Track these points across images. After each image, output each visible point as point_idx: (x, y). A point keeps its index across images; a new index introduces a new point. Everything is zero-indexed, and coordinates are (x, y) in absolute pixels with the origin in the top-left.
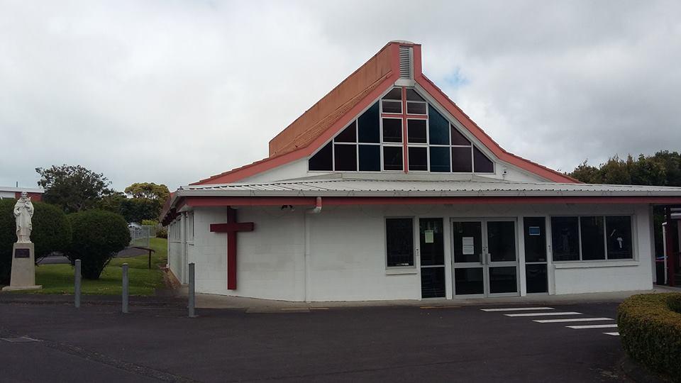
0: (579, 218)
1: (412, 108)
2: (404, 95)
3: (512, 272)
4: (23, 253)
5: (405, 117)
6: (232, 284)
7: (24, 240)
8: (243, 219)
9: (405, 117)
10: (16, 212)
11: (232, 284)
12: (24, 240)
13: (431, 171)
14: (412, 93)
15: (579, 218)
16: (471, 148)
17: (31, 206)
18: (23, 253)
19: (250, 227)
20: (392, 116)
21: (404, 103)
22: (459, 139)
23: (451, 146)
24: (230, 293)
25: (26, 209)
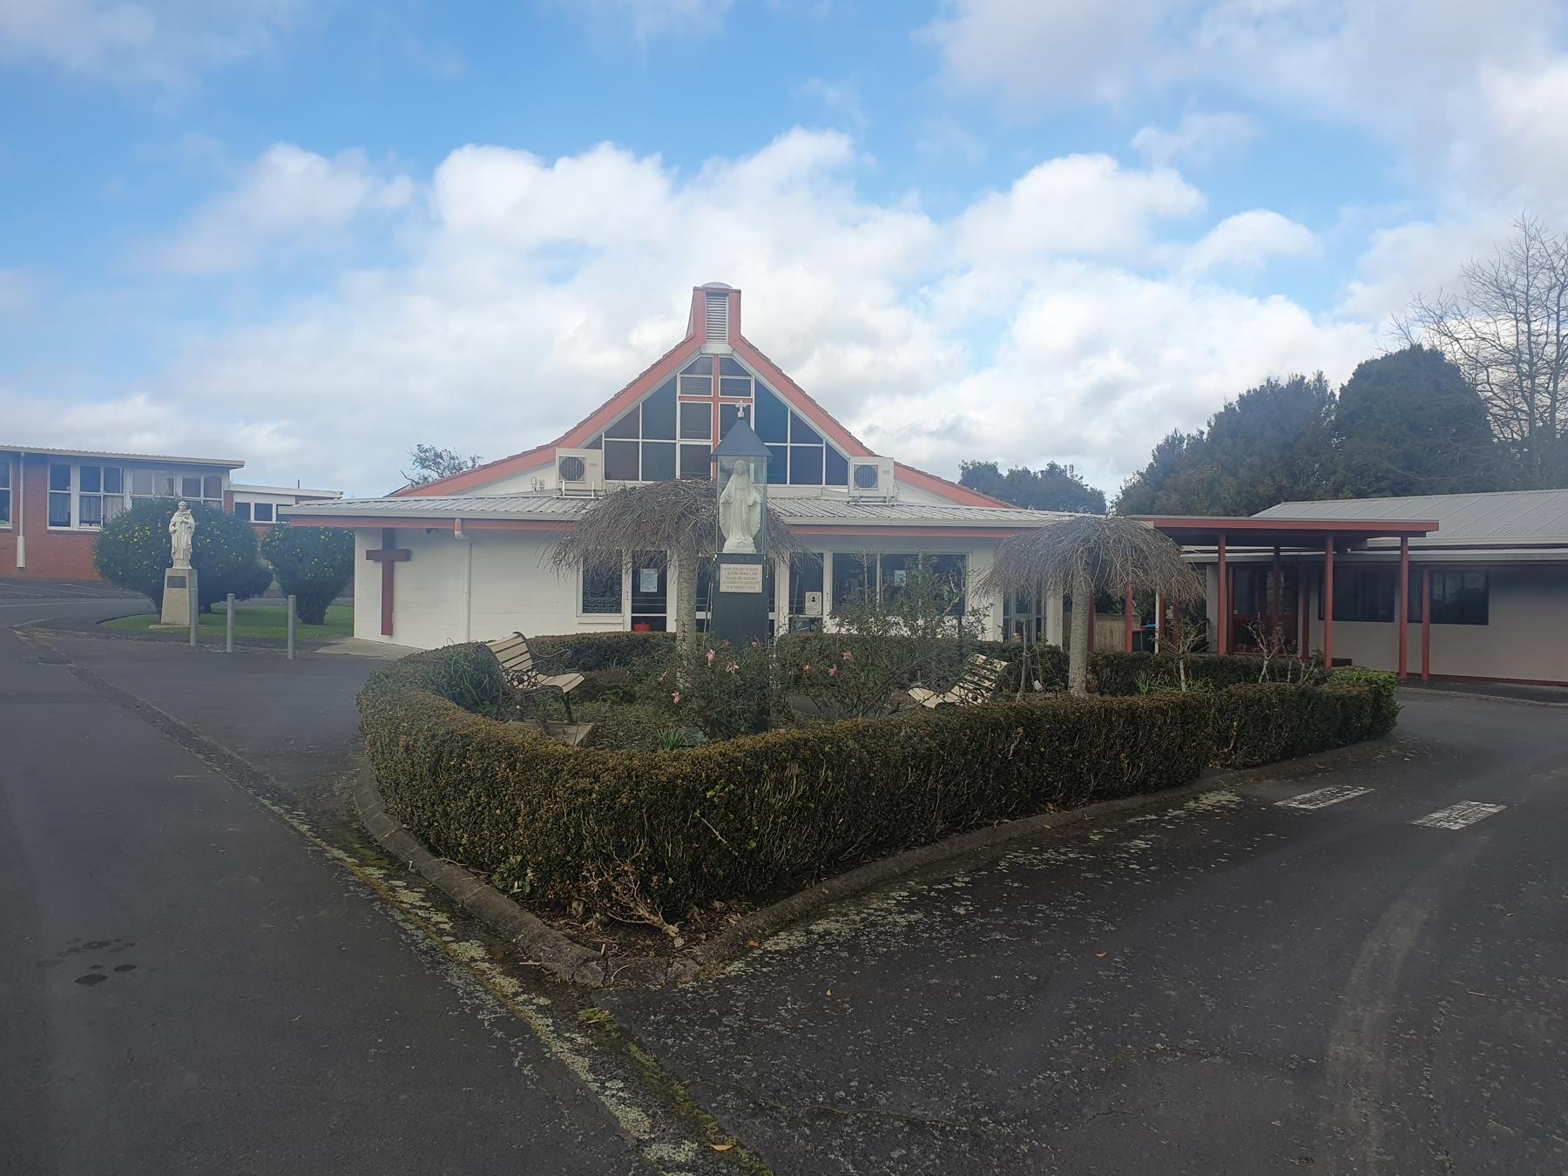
0: (634, 615)
1: (728, 388)
2: (716, 366)
3: (797, 604)
4: (178, 582)
5: (715, 400)
6: (388, 628)
7: (181, 565)
8: (400, 546)
9: (715, 400)
10: (171, 528)
11: (388, 628)
12: (181, 565)
13: (271, 505)
14: (729, 365)
15: (634, 615)
16: (822, 448)
17: (191, 520)
18: (178, 582)
19: (407, 556)
20: (697, 399)
21: (716, 380)
22: (803, 432)
23: (640, 440)
24: (385, 639)
25: (183, 524)
